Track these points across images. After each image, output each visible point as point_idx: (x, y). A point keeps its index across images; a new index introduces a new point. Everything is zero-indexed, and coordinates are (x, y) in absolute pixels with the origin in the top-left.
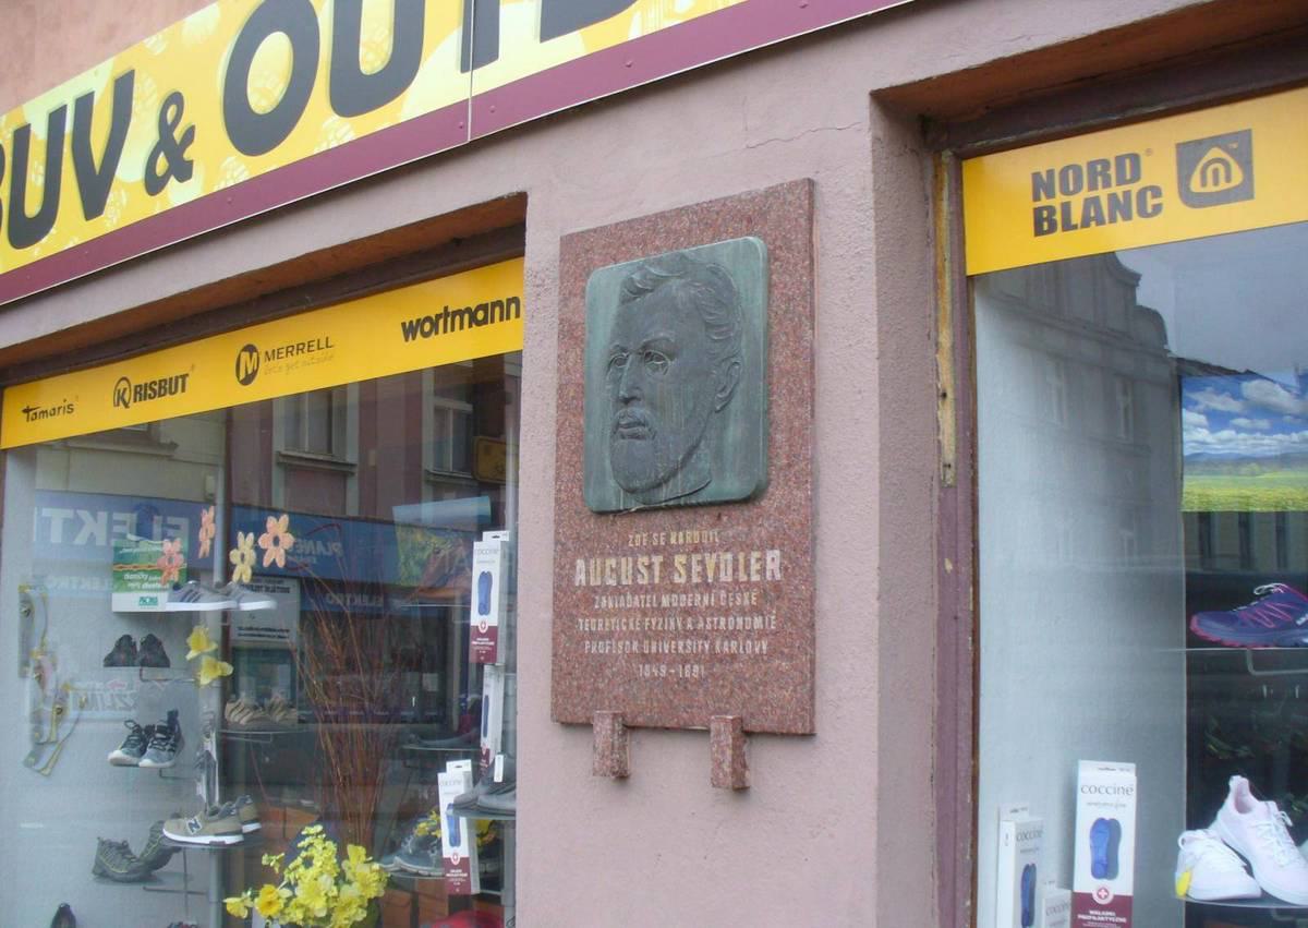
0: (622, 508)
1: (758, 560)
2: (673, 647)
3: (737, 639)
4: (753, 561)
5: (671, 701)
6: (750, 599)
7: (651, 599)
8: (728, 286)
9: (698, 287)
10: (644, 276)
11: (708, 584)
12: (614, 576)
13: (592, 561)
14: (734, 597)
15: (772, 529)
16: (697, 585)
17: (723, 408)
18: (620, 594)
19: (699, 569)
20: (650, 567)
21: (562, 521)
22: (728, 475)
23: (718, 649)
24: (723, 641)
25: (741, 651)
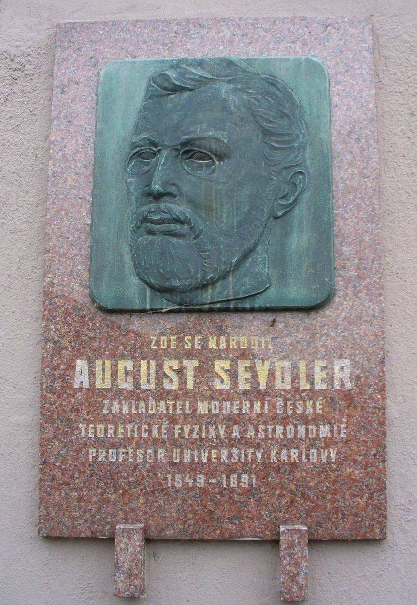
0: (148, 307)
1: (324, 368)
2: (214, 456)
3: (297, 448)
4: (317, 369)
5: (212, 512)
6: (314, 407)
7: (184, 405)
8: (290, 98)
9: (251, 94)
10: (182, 75)
11: (259, 392)
12: (130, 379)
13: (98, 363)
14: (294, 404)
15: (339, 339)
16: (245, 392)
17: (284, 215)
18: (139, 399)
19: (248, 375)
20: (180, 372)
21: (54, 317)
22: (291, 281)
23: (273, 458)
24: (280, 450)
25: (304, 460)
